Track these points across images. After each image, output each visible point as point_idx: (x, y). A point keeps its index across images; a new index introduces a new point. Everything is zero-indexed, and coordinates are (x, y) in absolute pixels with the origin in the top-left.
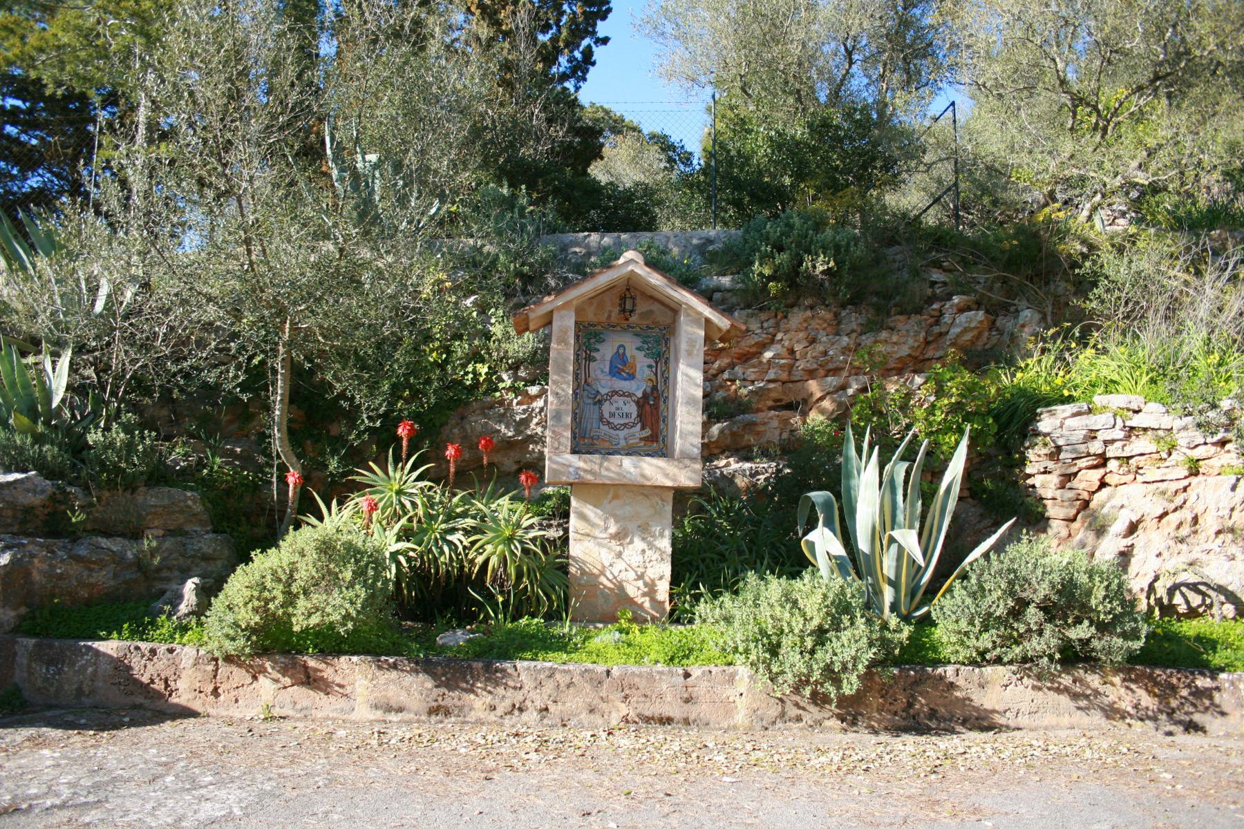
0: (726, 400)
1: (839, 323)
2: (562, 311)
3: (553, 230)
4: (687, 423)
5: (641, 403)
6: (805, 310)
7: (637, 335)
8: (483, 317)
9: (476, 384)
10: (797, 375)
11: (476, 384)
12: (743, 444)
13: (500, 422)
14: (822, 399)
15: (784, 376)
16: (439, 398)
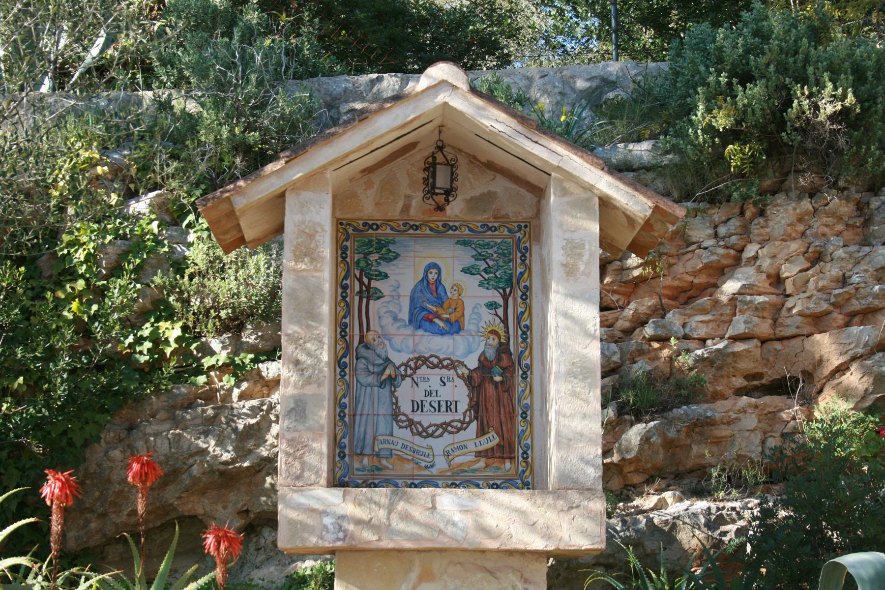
0: (651, 378)
1: (867, 222)
2: (307, 193)
3: (309, 71)
4: (571, 415)
5: (477, 381)
6: (800, 198)
7: (464, 243)
8: (173, 232)
9: (158, 360)
10: (791, 324)
11: (158, 360)
12: (690, 464)
13: (206, 434)
14: (841, 369)
15: (764, 328)
16: (74, 390)
